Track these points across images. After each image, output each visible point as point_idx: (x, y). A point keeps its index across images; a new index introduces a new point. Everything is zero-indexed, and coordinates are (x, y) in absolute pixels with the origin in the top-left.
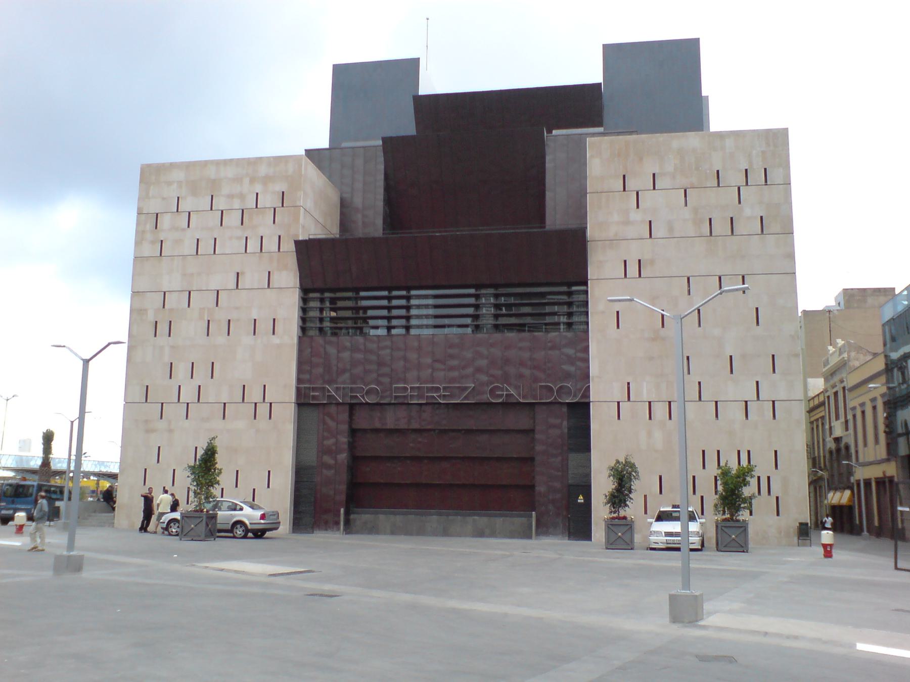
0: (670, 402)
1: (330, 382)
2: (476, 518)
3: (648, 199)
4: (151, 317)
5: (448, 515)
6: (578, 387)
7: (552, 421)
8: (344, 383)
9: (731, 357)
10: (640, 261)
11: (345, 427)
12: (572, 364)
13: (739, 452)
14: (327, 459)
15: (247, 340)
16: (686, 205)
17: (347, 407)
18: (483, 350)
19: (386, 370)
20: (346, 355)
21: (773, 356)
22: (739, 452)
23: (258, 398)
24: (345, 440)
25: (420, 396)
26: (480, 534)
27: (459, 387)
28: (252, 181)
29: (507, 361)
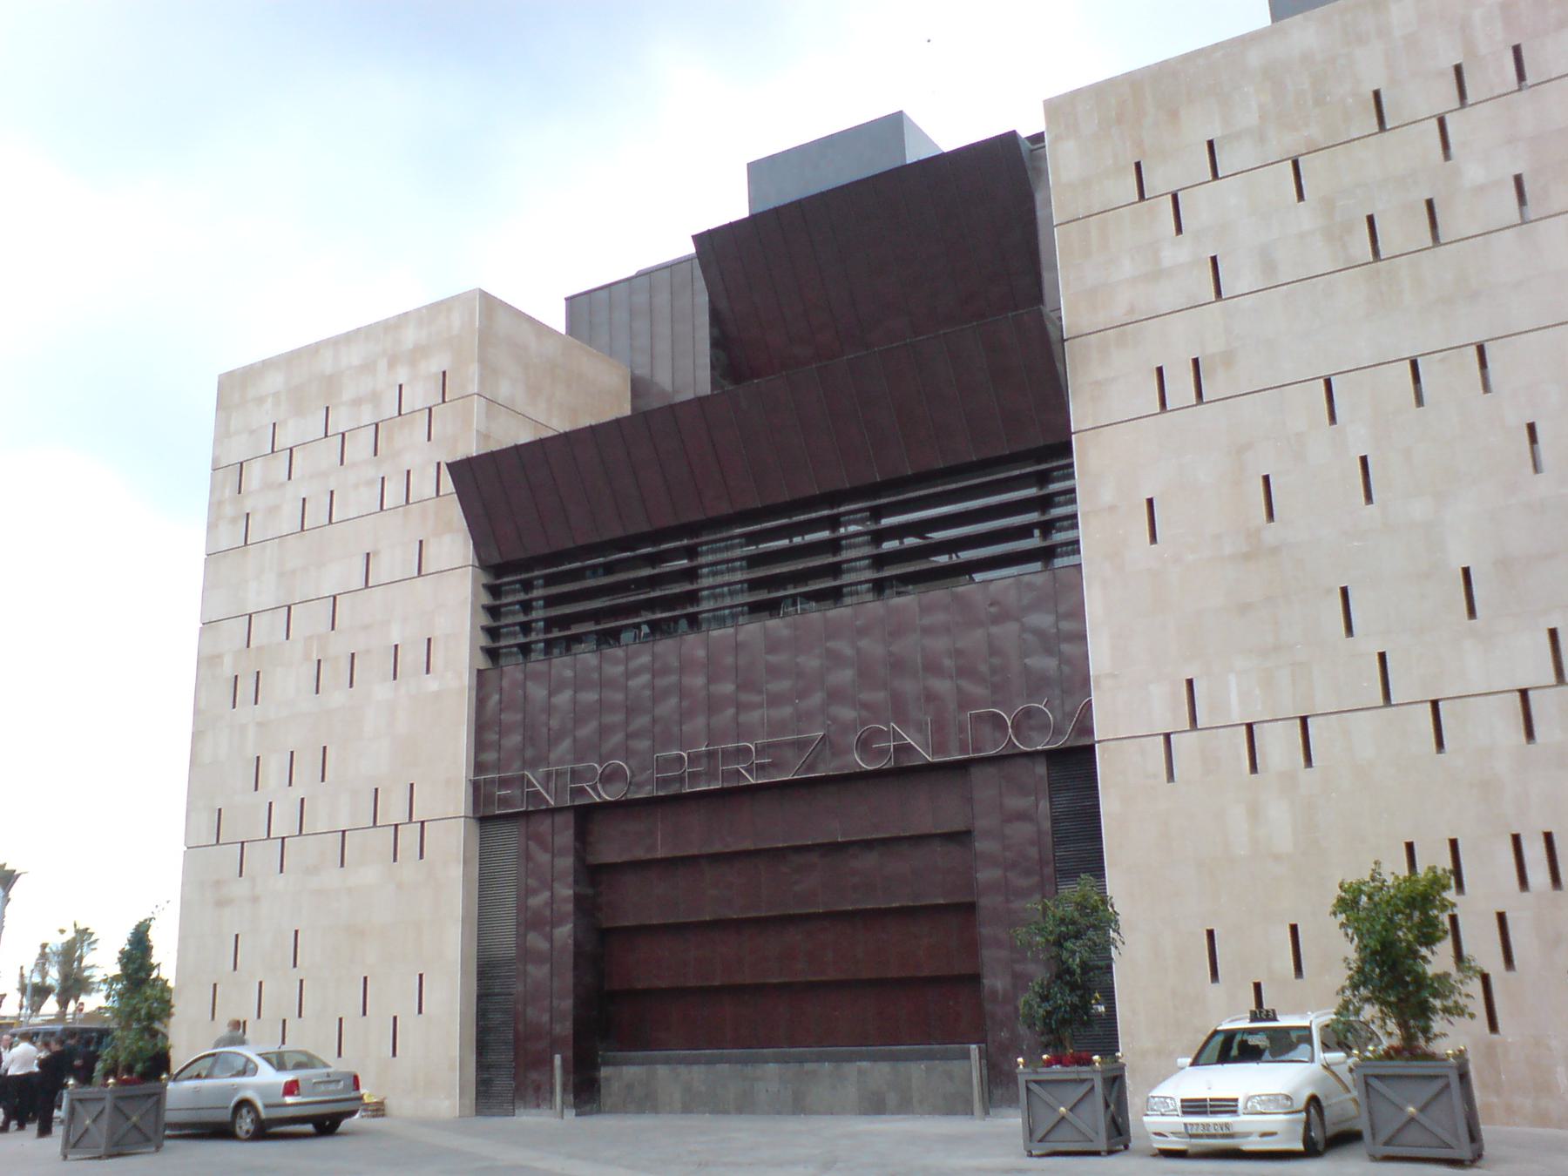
0: (1304, 720)
1: (532, 764)
2: (864, 1064)
3: (1199, 207)
4: (227, 670)
5: (801, 1060)
6: (1068, 708)
7: (1015, 803)
8: (561, 761)
9: (1466, 572)
10: (1196, 362)
11: (567, 863)
12: (1049, 652)
13: (1516, 839)
14: (536, 941)
15: (383, 691)
16: (1301, 196)
17: (570, 818)
18: (844, 647)
19: (642, 721)
20: (563, 698)
21: (1344, 591)
22: (1516, 839)
23: (400, 815)
24: (568, 892)
25: (711, 775)
26: (875, 1105)
27: (793, 744)
28: (393, 362)
29: (898, 665)
